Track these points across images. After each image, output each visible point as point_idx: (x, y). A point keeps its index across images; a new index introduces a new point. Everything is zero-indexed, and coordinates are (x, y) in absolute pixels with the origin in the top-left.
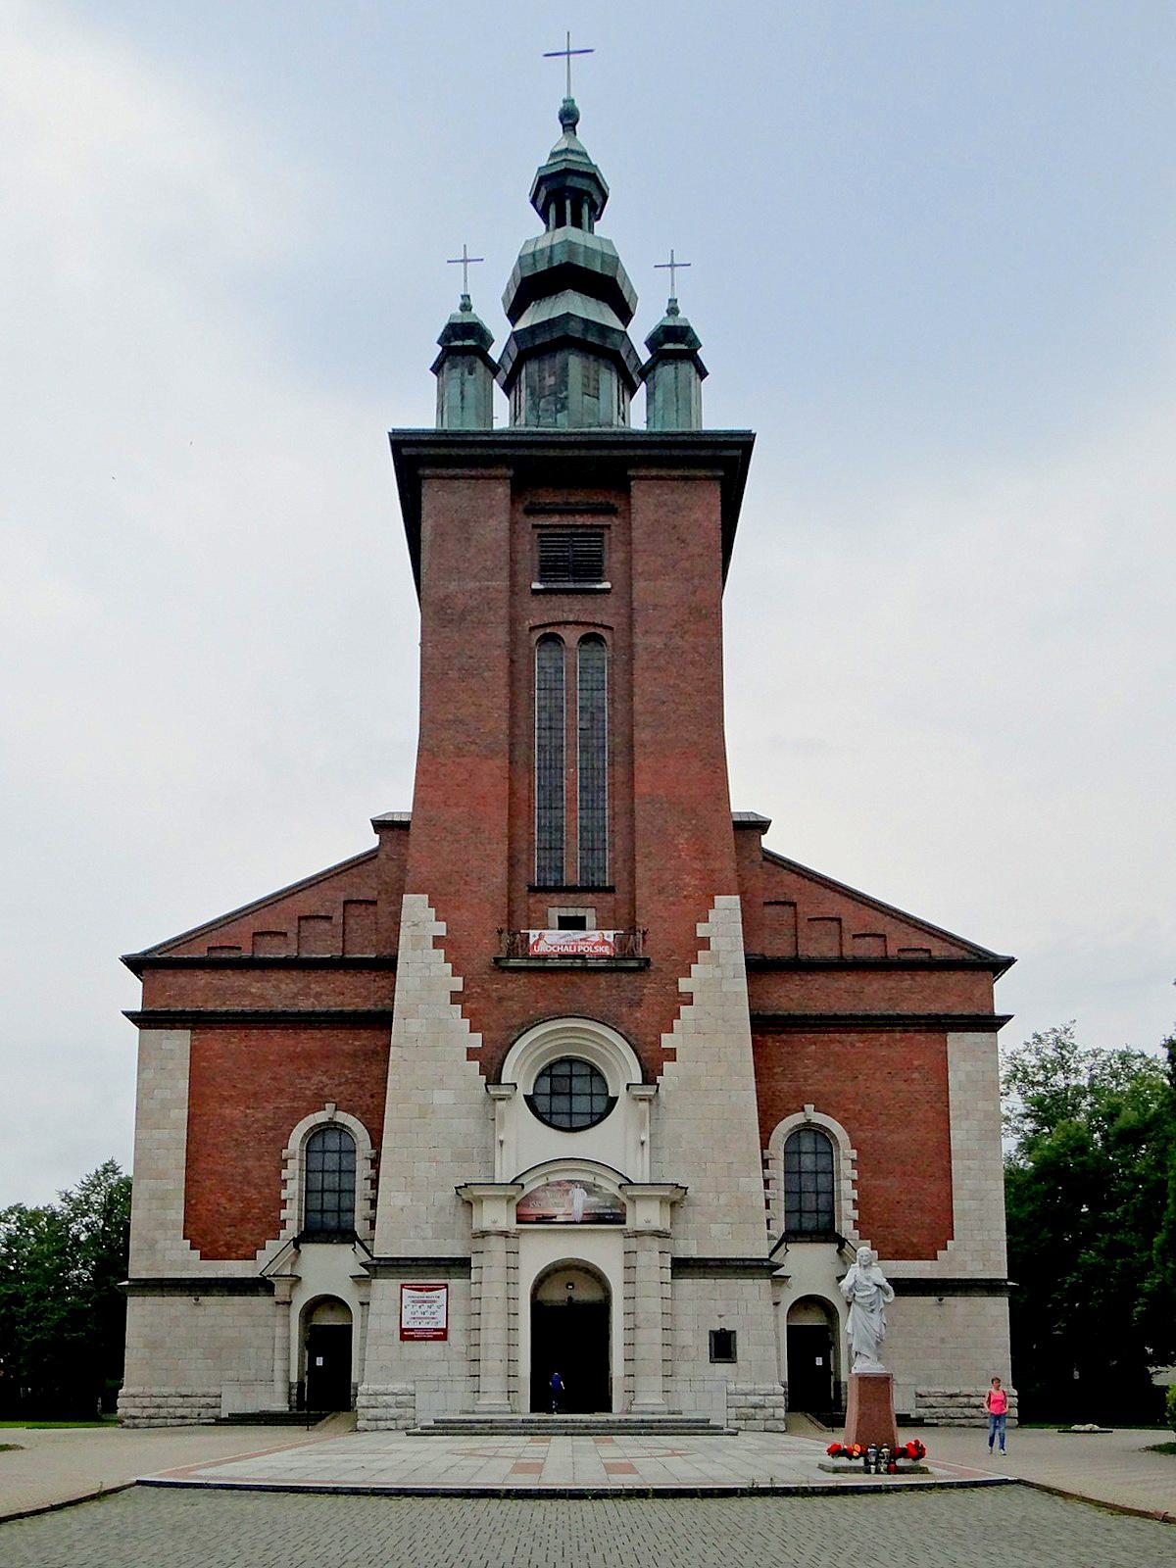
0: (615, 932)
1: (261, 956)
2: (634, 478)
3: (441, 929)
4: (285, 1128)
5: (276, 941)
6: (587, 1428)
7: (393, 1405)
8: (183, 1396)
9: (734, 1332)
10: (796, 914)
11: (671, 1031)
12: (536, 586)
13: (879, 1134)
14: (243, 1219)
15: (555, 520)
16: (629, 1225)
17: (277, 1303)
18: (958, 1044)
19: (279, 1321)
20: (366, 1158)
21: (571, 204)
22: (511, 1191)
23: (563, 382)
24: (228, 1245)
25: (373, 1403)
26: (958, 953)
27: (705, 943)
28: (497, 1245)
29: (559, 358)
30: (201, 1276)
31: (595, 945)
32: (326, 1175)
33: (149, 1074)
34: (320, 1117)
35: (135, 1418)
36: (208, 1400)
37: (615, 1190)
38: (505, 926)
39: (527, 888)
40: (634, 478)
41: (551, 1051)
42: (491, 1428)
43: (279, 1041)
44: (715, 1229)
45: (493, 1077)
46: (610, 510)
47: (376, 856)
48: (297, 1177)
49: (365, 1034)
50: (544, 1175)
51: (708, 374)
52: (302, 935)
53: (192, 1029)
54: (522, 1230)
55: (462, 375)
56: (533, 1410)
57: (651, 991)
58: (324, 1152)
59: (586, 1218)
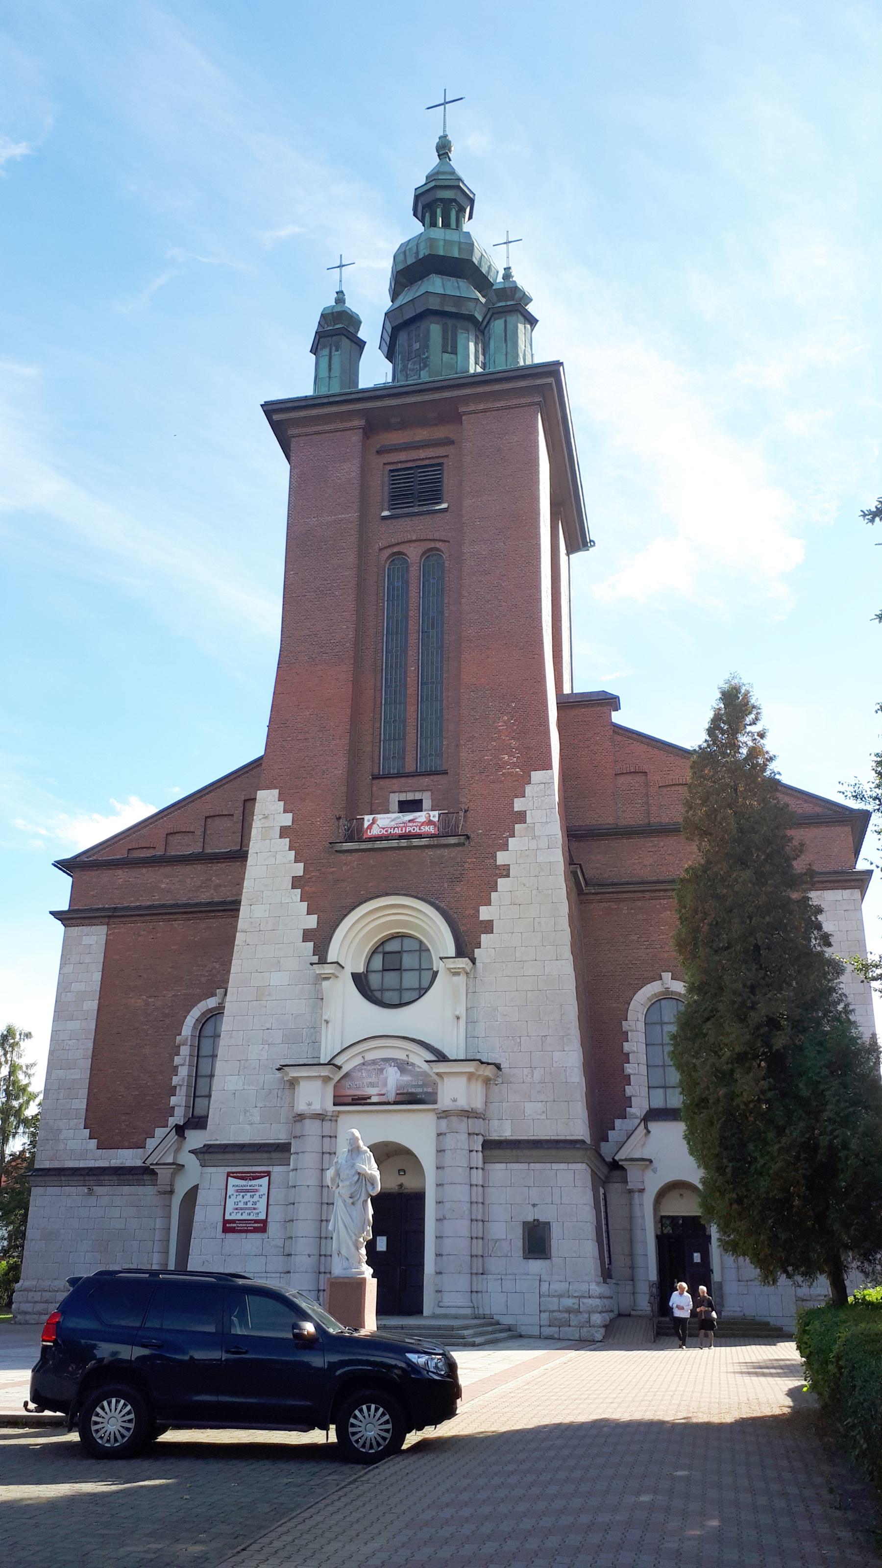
0: (440, 812)
9: (549, 1223)
10: (647, 785)
11: (488, 903)
12: (386, 513)
23: (426, 346)
27: (521, 817)
28: (312, 1128)
30: (97, 1165)
31: (422, 825)
35: (26, 1313)
38: (343, 814)
40: (465, 413)
44: (531, 1108)
45: (321, 954)
51: (532, 300)
54: (339, 1112)
55: (330, 352)
59: (399, 1099)
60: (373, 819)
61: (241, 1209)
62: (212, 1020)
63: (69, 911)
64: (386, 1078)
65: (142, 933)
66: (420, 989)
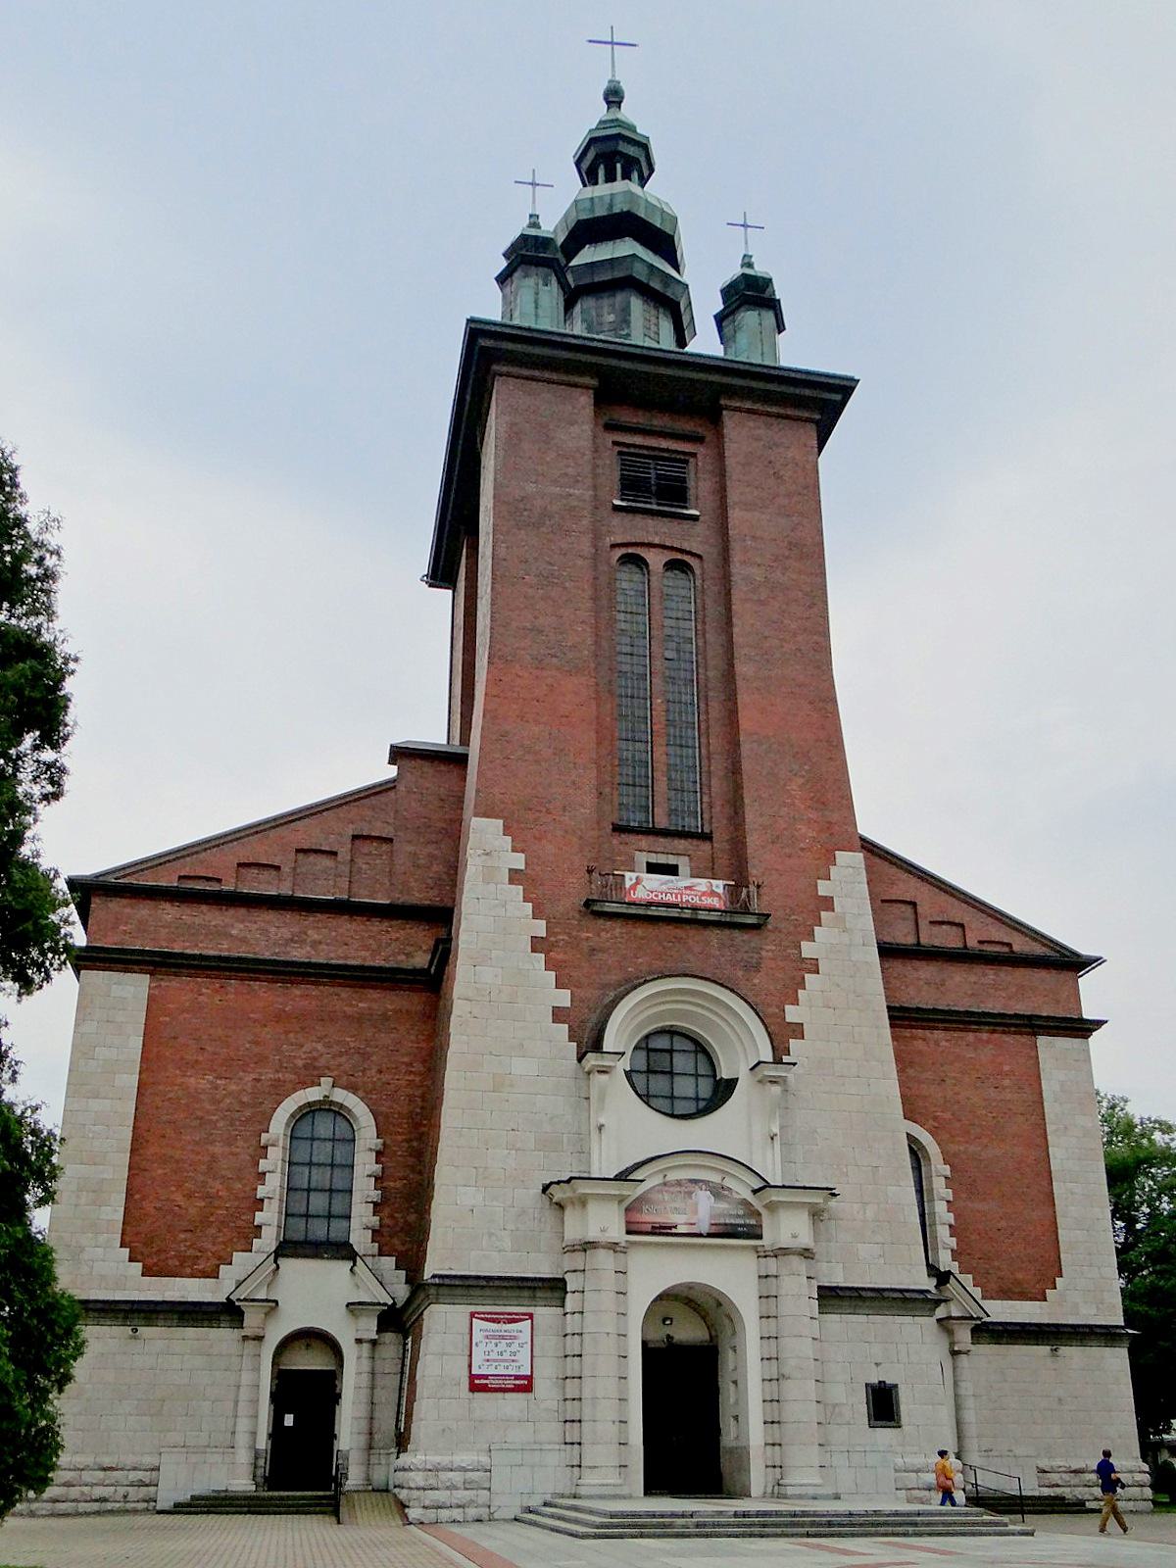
1: (245, 891)
2: (727, 408)
3: (519, 861)
4: (267, 1105)
5: (266, 875)
6: (830, 1524)
7: (459, 1485)
8: (104, 1469)
9: (896, 1386)
11: (796, 1002)
12: (617, 502)
13: (972, 1148)
14: (205, 1221)
15: (638, 440)
16: (767, 1241)
17: (245, 1338)
18: (1049, 1048)
19: (247, 1362)
20: (371, 1150)
21: (622, 167)
22: (615, 1189)
24: (183, 1260)
25: (432, 1482)
26: (1039, 950)
27: (828, 903)
29: (620, 297)
32: (314, 1171)
33: (89, 1027)
34: (313, 1094)
36: (140, 1475)
37: (749, 1196)
39: (611, 827)
40: (727, 408)
41: (660, 1016)
42: (698, 1526)
43: (265, 995)
44: (864, 1250)
45: (591, 1042)
46: (698, 439)
47: (394, 787)
48: (279, 1170)
49: (374, 994)
50: (661, 1171)
52: (298, 871)
53: (152, 974)
55: (537, 285)
56: (652, 1487)
57: (770, 954)
58: (313, 1139)
59: (714, 1230)
60: (637, 878)
61: (495, 1361)
62: (309, 1118)
63: (87, 947)
64: (696, 1204)
65: (204, 990)
66: (648, 1096)
